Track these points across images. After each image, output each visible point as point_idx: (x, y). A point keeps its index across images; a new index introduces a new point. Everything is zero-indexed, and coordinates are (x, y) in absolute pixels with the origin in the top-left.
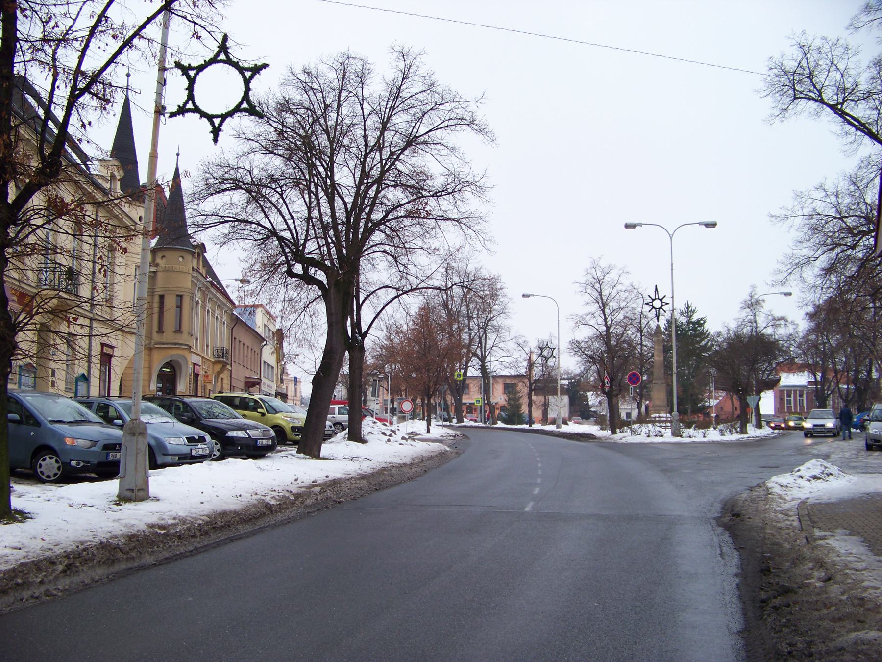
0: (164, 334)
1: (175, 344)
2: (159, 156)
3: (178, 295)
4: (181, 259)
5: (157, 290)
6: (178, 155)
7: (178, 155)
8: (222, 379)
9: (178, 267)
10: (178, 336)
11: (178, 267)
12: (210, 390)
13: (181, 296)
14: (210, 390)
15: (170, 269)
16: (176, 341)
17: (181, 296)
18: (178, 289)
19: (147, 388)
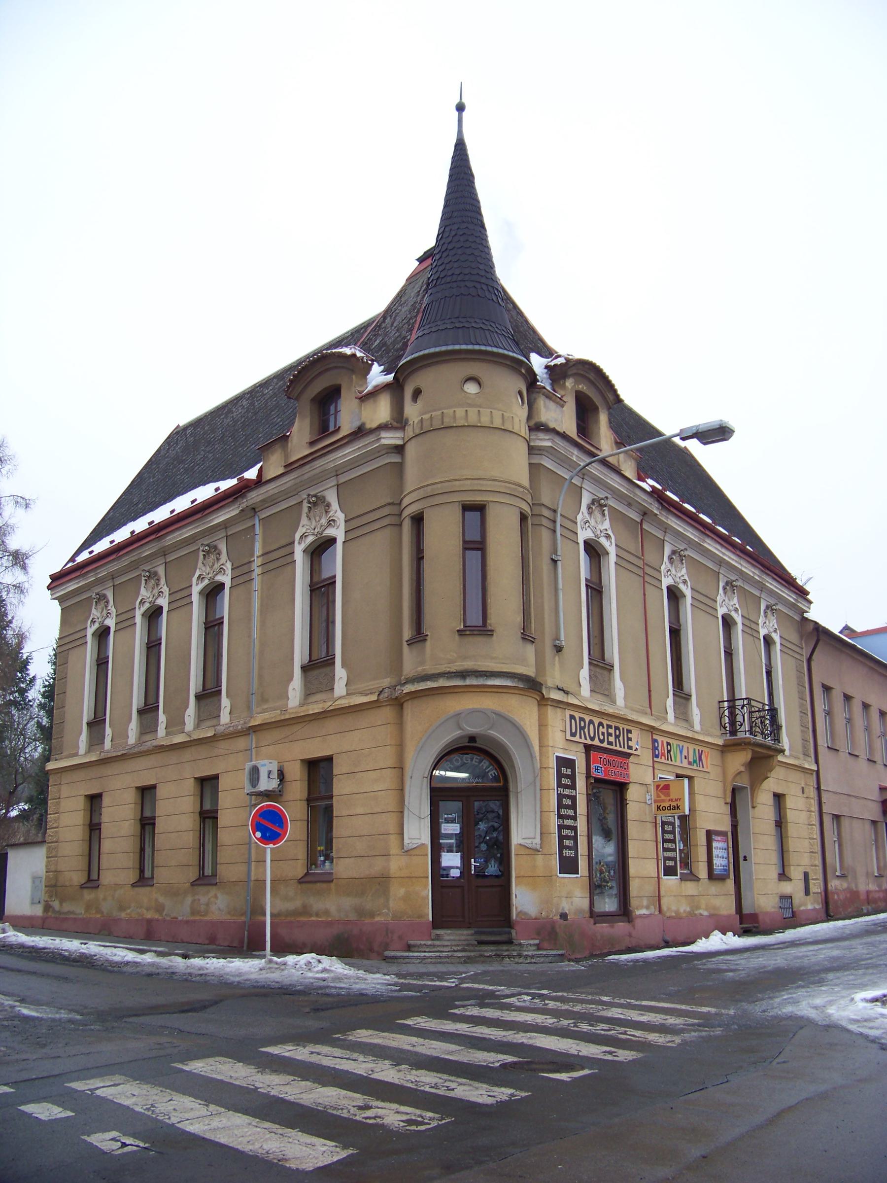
0: (428, 644)
1: (463, 674)
2: (818, 621)
3: (467, 508)
4: (471, 388)
5: (406, 502)
6: (460, 108)
7: (460, 108)
8: (779, 798)
9: (460, 412)
10: (477, 644)
11: (460, 412)
12: (709, 834)
13: (480, 508)
14: (709, 834)
15: (437, 424)
16: (468, 665)
17: (480, 508)
18: (468, 485)
19: (393, 840)
